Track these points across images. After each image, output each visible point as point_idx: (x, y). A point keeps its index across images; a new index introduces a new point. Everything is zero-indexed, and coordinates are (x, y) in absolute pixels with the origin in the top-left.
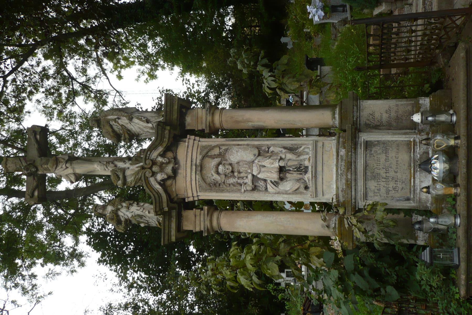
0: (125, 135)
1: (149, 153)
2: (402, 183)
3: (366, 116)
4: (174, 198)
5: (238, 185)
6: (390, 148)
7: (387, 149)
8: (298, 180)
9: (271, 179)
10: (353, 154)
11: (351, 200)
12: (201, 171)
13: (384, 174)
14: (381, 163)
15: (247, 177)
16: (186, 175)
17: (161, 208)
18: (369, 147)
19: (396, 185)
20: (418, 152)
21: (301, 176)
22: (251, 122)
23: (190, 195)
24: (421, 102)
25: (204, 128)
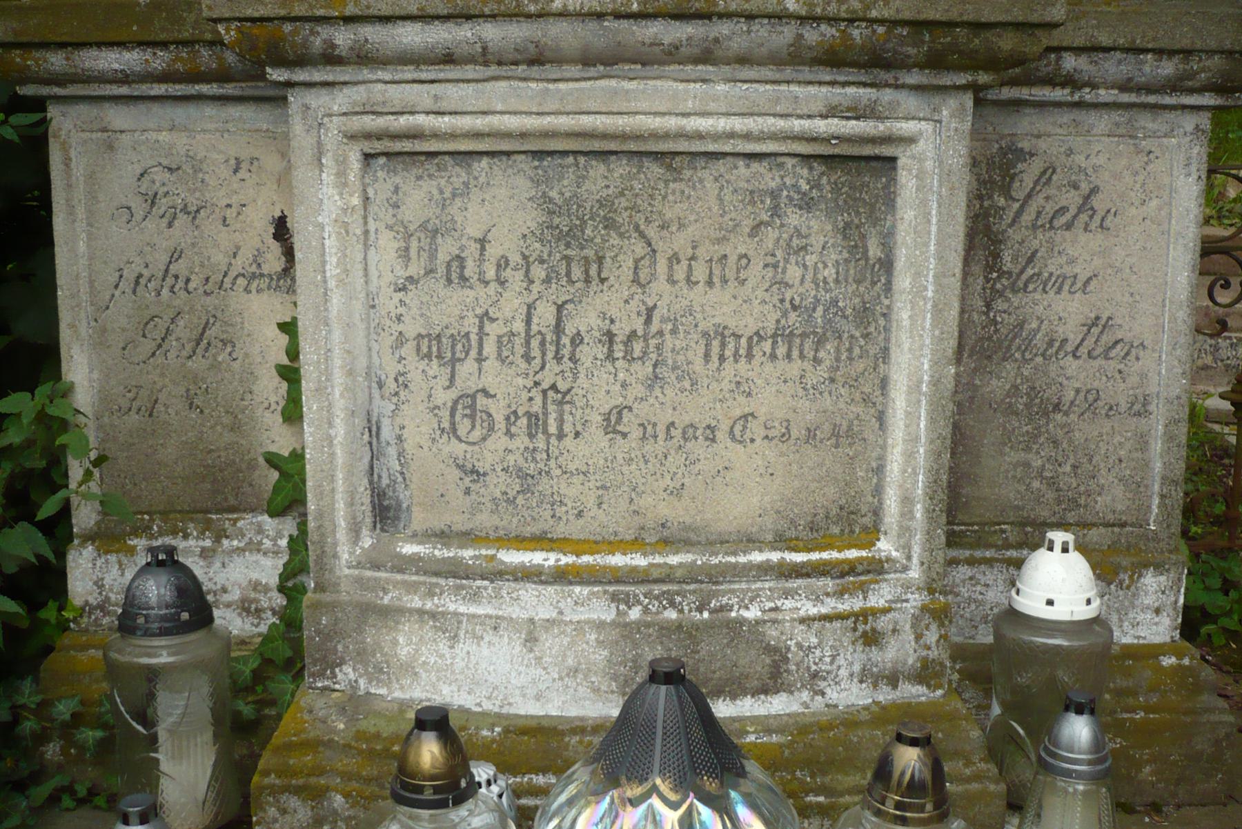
2: (522, 475)
3: (1080, 159)
6: (822, 372)
7: (820, 343)
10: (786, 34)
11: (349, 20)
13: (595, 321)
14: (697, 295)
18: (836, 188)
19: (499, 417)
20: (788, 604)
24: (1151, 582)
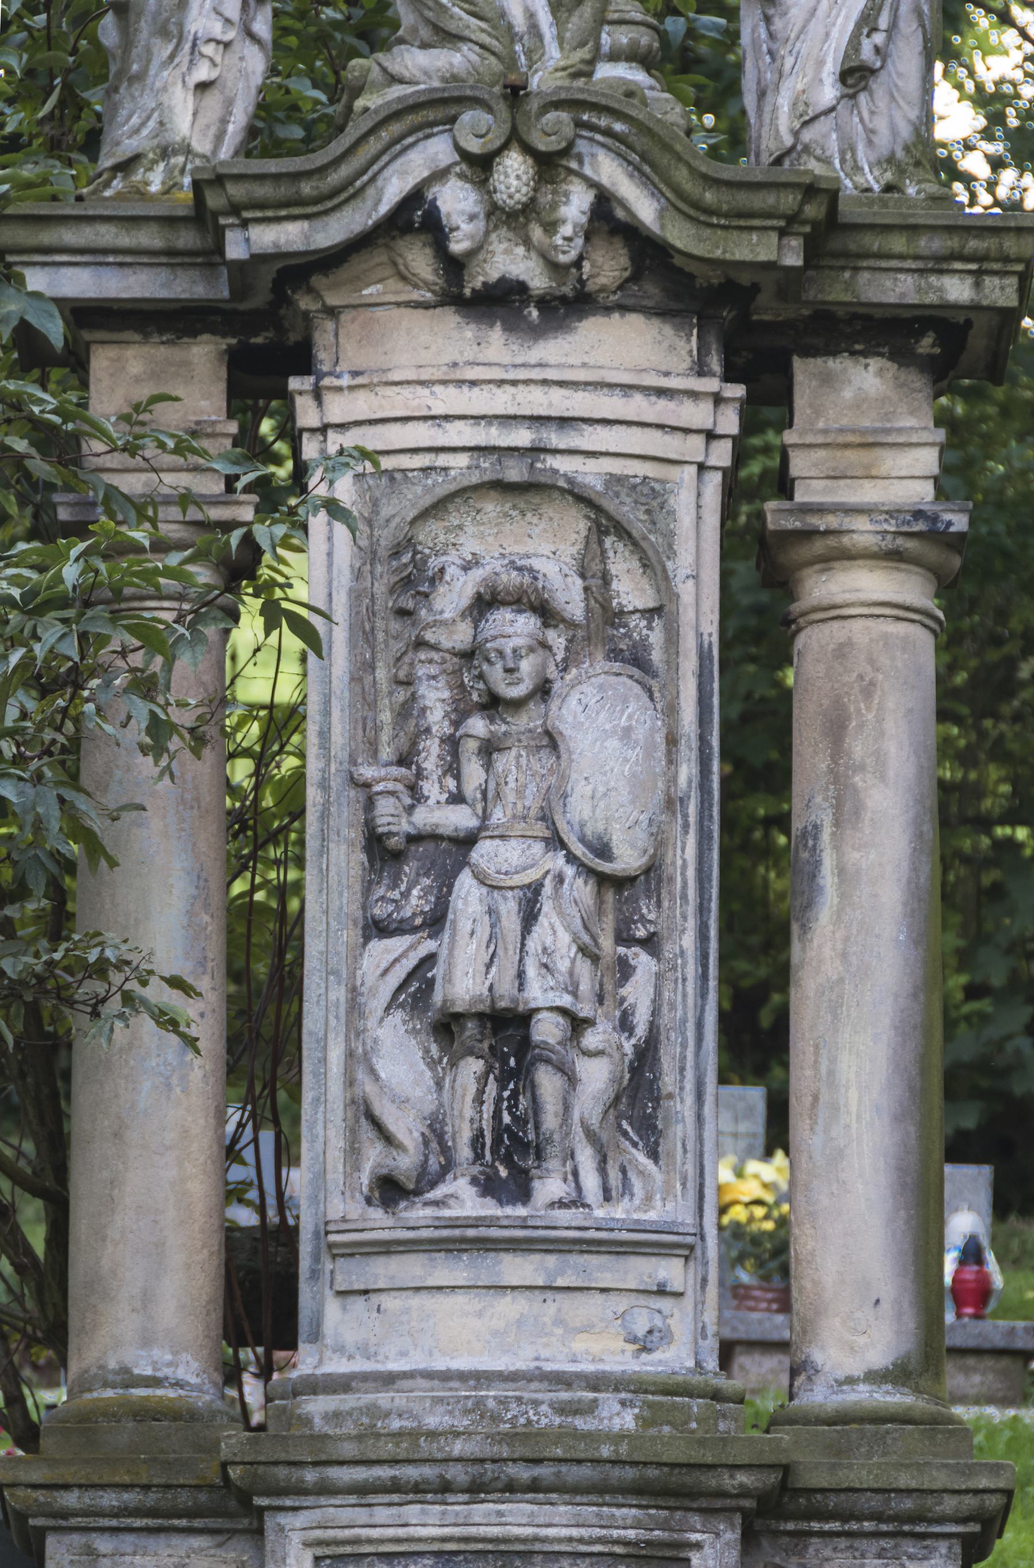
1: (618, 127)
4: (311, 291)
5: (403, 741)
9: (443, 954)
11: (316, 1464)
12: (501, 487)
15: (457, 798)
16: (473, 383)
17: (247, 214)
21: (464, 1152)
22: (837, 823)
23: (337, 409)
25: (800, 496)
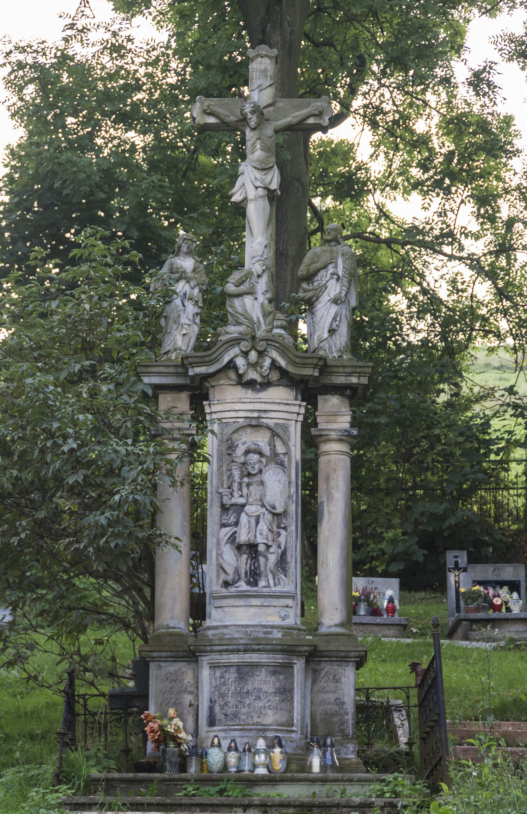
0: (310, 291)
8: (237, 571)
12: (251, 426)
15: (241, 496)
21: (243, 576)
23: (214, 408)
